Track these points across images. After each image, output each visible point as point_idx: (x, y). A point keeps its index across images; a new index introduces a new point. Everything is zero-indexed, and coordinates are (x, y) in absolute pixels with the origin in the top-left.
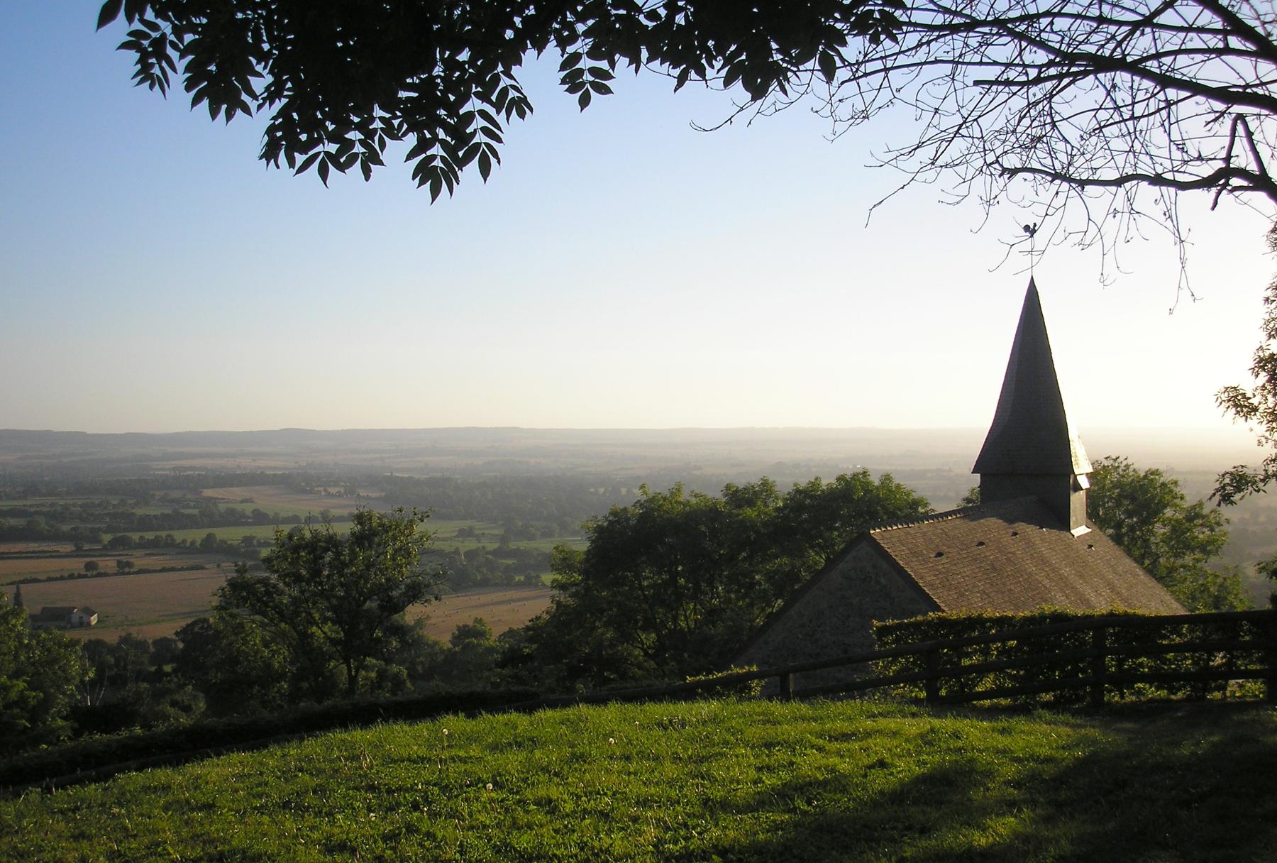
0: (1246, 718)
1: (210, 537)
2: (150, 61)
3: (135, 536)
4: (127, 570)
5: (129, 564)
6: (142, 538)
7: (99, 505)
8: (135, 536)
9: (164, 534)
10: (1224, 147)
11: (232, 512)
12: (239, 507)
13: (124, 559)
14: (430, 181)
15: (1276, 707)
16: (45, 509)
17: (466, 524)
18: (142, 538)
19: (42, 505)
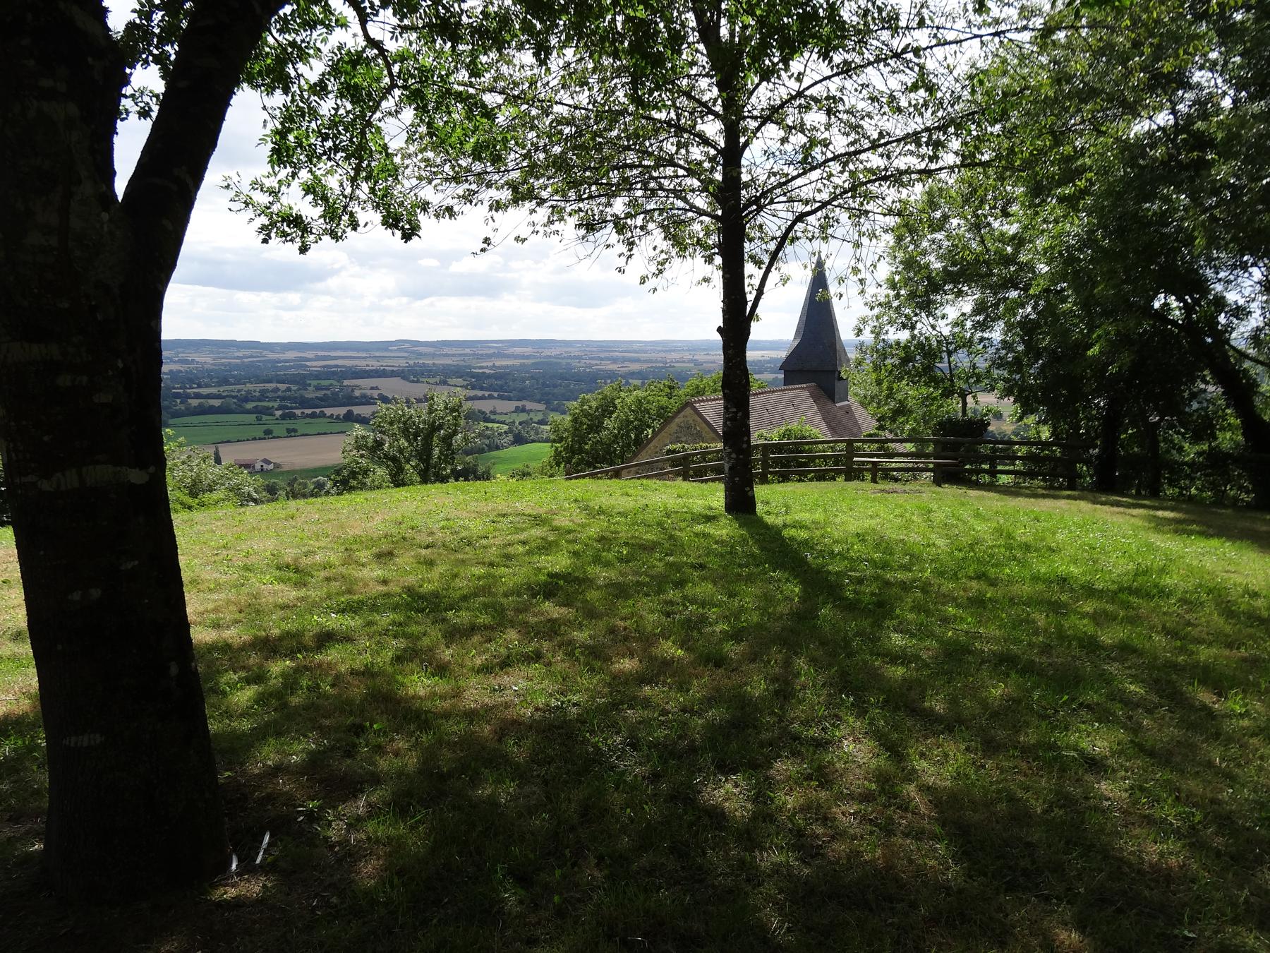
0: (1248, 524)
1: (350, 412)
2: (1157, 305)
3: (298, 412)
4: (293, 434)
5: (295, 430)
6: (303, 413)
7: (272, 391)
8: (298, 412)
9: (318, 411)
10: (265, 121)
11: (364, 396)
12: (369, 392)
13: (291, 427)
14: (120, 186)
15: (1268, 517)
16: (234, 394)
17: (520, 404)
18: (303, 413)
19: (232, 391)
